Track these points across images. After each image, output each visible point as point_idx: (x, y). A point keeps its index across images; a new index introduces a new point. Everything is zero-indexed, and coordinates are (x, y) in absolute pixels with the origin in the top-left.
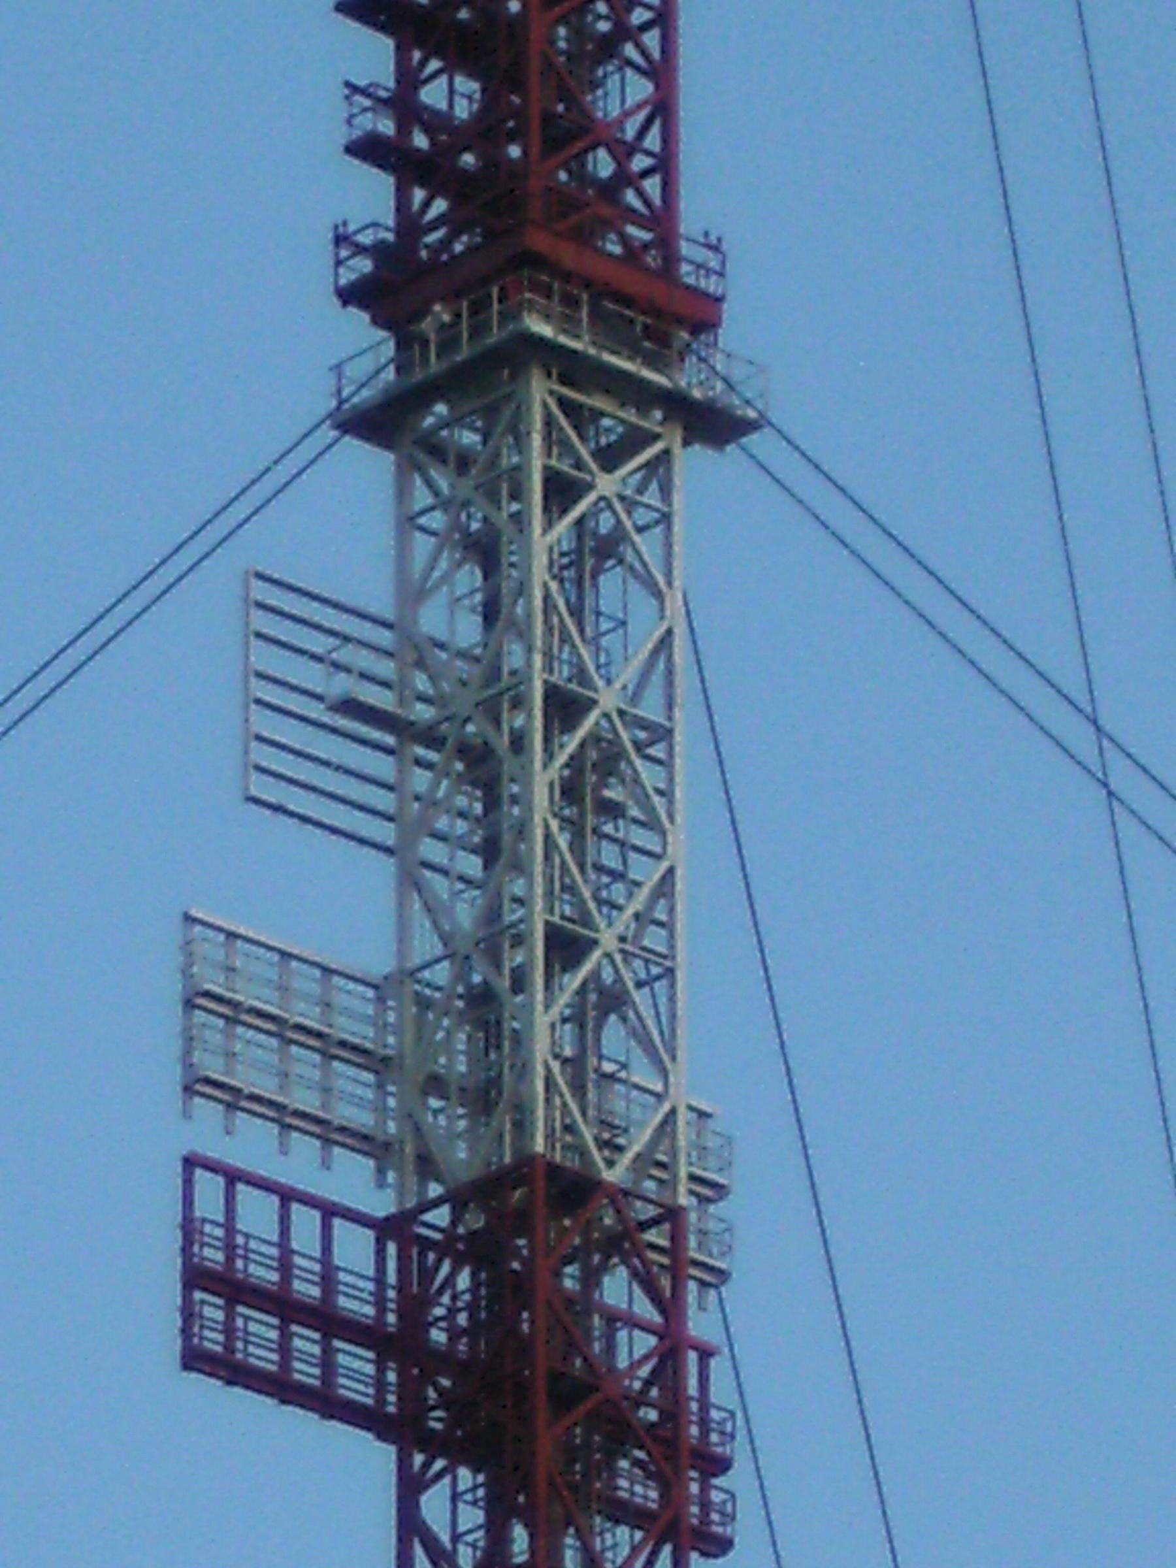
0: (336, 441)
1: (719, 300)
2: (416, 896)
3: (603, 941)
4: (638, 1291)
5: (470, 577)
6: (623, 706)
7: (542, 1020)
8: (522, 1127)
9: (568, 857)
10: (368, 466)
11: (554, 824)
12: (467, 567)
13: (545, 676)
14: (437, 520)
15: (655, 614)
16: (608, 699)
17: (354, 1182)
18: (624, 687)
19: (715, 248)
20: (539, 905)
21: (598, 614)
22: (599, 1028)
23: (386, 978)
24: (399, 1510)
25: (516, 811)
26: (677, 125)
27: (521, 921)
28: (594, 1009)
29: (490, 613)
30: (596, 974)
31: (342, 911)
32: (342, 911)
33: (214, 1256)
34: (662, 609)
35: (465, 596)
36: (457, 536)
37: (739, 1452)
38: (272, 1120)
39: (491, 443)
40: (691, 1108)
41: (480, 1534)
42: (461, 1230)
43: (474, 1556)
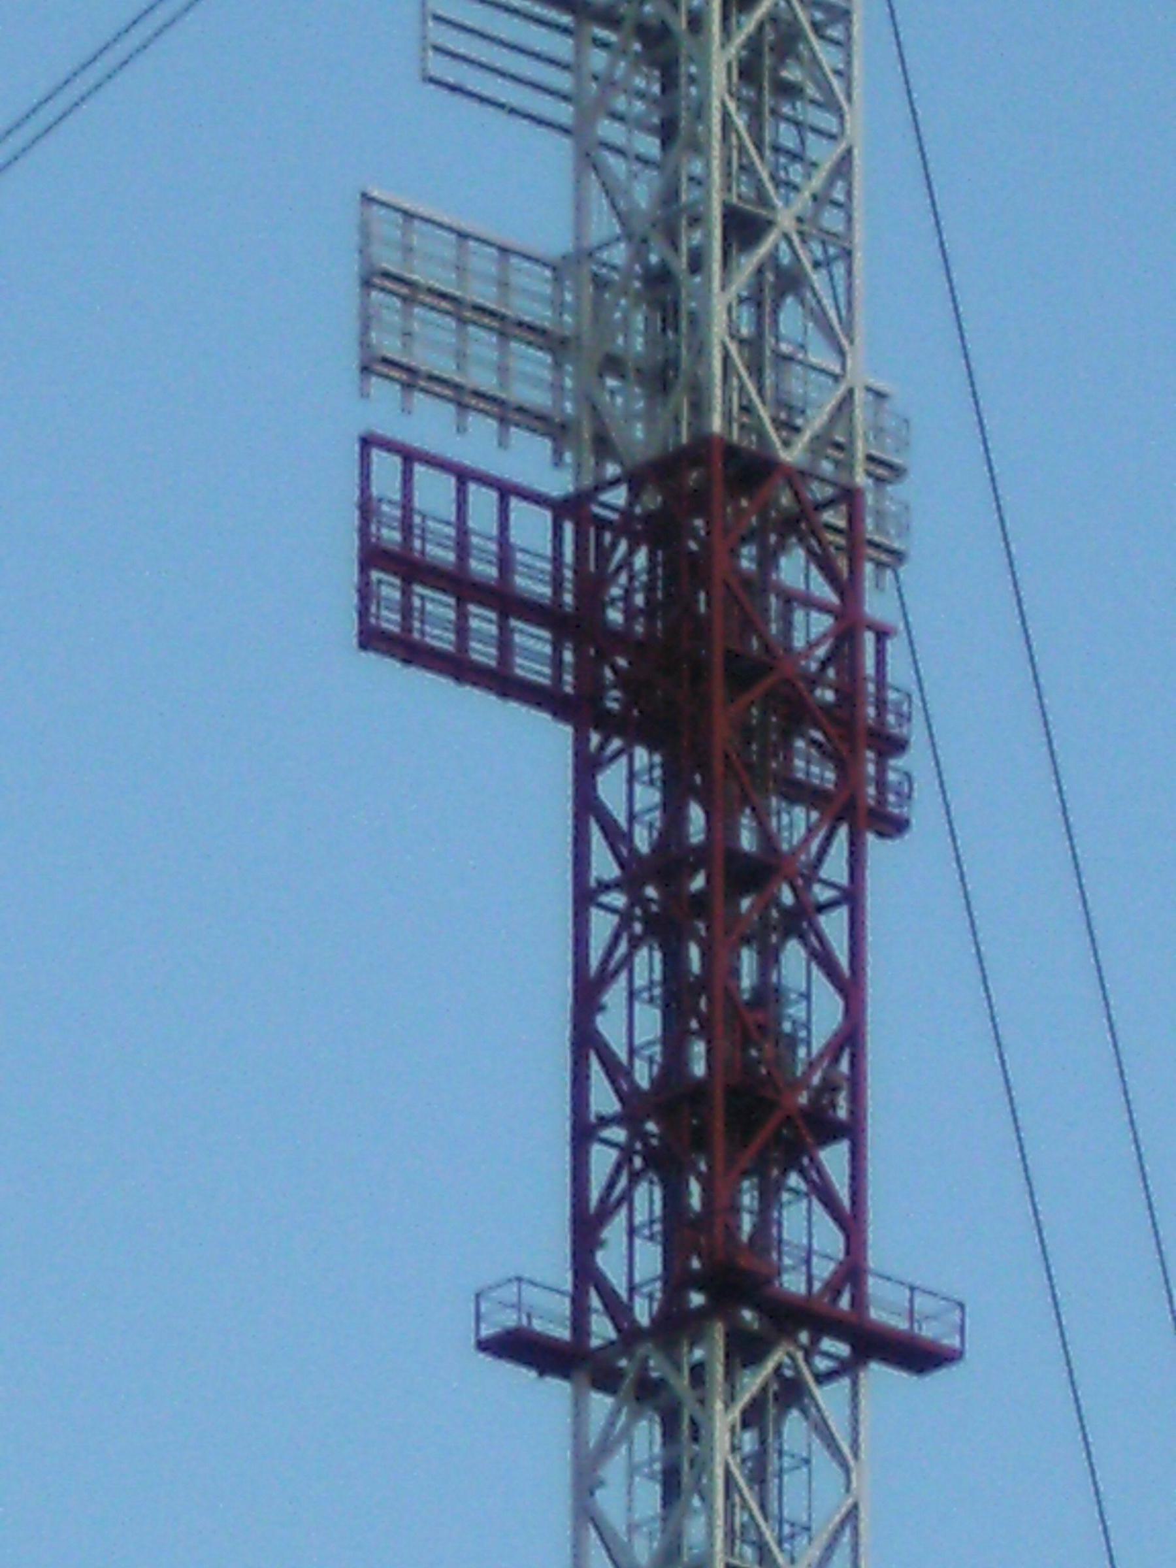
2: (593, 176)
4: (816, 972)
8: (699, 408)
11: (732, 106)
17: (531, 461)
23: (564, 257)
25: (693, 90)
31: (520, 190)
32: (520, 190)
33: (391, 536)
37: (916, 734)
38: (450, 400)
40: (869, 389)
43: (651, 1548)
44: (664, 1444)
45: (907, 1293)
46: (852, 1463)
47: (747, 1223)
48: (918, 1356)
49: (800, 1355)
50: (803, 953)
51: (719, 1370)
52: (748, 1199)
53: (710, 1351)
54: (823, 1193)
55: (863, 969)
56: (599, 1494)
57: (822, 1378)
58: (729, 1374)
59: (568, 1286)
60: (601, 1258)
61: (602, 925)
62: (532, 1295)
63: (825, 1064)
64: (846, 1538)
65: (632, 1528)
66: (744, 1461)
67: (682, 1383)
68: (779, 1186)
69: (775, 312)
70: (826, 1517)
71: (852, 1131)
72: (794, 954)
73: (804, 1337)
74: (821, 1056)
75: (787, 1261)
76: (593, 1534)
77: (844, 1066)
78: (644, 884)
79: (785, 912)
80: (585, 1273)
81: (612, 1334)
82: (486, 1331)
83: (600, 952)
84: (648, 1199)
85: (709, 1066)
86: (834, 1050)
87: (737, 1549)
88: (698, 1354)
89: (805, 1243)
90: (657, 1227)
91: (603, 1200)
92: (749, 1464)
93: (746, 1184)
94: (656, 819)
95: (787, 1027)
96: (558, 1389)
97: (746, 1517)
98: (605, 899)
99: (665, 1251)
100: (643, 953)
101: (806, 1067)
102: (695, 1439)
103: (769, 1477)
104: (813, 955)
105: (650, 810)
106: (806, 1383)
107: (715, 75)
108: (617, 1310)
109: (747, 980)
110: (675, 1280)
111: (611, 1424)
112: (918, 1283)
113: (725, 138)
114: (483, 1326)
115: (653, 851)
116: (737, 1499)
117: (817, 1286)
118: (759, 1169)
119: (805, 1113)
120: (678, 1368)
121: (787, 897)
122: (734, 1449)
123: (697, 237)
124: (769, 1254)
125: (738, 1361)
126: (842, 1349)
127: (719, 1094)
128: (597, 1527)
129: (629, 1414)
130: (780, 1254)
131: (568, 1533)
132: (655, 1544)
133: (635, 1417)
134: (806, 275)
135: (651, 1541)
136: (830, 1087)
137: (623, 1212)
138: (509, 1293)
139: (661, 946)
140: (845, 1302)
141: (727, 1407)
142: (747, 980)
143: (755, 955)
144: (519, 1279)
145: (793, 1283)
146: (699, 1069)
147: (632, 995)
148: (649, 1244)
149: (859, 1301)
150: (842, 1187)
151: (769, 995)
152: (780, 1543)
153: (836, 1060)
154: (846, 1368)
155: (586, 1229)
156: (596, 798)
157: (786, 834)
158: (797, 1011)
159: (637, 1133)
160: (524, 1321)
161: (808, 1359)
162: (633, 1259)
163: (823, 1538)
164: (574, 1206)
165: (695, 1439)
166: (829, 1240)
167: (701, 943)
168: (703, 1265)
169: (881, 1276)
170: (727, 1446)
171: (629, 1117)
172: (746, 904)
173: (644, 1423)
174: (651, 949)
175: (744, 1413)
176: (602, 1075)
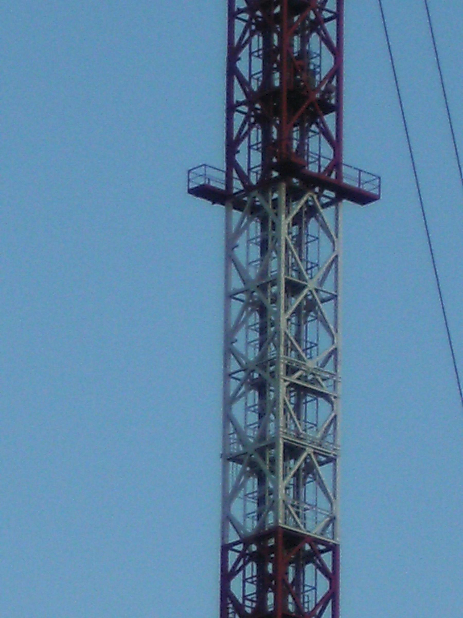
3: (309, 286)
4: (323, 45)
5: (253, 396)
6: (316, 287)
7: (282, 485)
9: (293, 413)
12: (251, 478)
13: (286, 277)
14: (241, 375)
15: (330, 343)
16: (311, 285)
18: (318, 279)
21: (308, 235)
22: (305, 478)
25: (273, 329)
26: (339, 566)
27: (275, 358)
29: (264, 247)
30: (306, 296)
34: (333, 406)
36: (249, 380)
39: (263, 349)
41: (259, 168)
42: (247, 552)
43: (258, 84)
44: (262, 231)
45: (358, 172)
46: (335, 239)
47: (295, 144)
48: (362, 198)
49: (315, 197)
50: (318, 39)
51: (283, 295)
52: (295, 135)
53: (280, 195)
54: (325, 132)
56: (237, 156)
57: (324, 206)
58: (287, 202)
59: (225, 169)
60: (239, 64)
61: (239, 26)
62: (210, 172)
63: (327, 82)
66: (293, 237)
67: (269, 207)
68: (308, 130)
69: (306, 223)
70: (325, 263)
71: (337, 108)
72: (314, 39)
73: (317, 189)
74: (325, 78)
75: (310, 160)
76: (231, 526)
77: (334, 83)
78: (257, 10)
79: (311, 21)
80: (231, 163)
81: (242, 188)
82: (192, 186)
84: (256, 135)
85: (281, 83)
86: (330, 76)
87: (290, 273)
88: (275, 196)
89: (318, 152)
91: (234, 567)
92: (295, 239)
93: (295, 129)
95: (312, 67)
96: (219, 209)
97: (293, 260)
98: (240, 108)
101: (319, 83)
102: (274, 229)
104: (318, 567)
105: (257, 167)
106: (315, 465)
108: (244, 178)
109: (296, 48)
110: (266, 166)
111: (242, 222)
112: (362, 169)
113: (286, 252)
114: (190, 184)
115: (257, 183)
116: (290, 253)
117: (322, 169)
118: (299, 123)
119: (319, 101)
120: (268, 202)
121: (312, 16)
122: (289, 233)
124: (304, 157)
125: (290, 294)
126: (332, 195)
127: (285, 94)
129: (248, 219)
130: (308, 156)
131: (222, 409)
132: (258, 271)
133: (250, 221)
134: (316, 467)
135: (254, 431)
136: (328, 91)
137: (247, 47)
138: (201, 171)
139: (262, 127)
140: (333, 176)
141: (286, 217)
142: (296, 48)
143: (299, 39)
144: (205, 165)
145: (313, 168)
146: (277, 83)
147: (250, 147)
148: (252, 585)
149: (339, 176)
150: (329, 607)
151: (305, 54)
153: (330, 82)
154: (334, 202)
155: (232, 147)
156: (230, 591)
157: (306, 605)
158: (316, 61)
159: (252, 108)
160: (207, 181)
161: (318, 198)
162: (250, 158)
163: (324, 269)
164: (227, 137)
165: (274, 229)
166: (327, 151)
167: (279, 34)
168: (277, 161)
169: (348, 166)
170: (286, 231)
171: (249, 102)
172: (296, 18)
173: (252, 391)
174: (259, 36)
175: (293, 219)
176: (239, 86)
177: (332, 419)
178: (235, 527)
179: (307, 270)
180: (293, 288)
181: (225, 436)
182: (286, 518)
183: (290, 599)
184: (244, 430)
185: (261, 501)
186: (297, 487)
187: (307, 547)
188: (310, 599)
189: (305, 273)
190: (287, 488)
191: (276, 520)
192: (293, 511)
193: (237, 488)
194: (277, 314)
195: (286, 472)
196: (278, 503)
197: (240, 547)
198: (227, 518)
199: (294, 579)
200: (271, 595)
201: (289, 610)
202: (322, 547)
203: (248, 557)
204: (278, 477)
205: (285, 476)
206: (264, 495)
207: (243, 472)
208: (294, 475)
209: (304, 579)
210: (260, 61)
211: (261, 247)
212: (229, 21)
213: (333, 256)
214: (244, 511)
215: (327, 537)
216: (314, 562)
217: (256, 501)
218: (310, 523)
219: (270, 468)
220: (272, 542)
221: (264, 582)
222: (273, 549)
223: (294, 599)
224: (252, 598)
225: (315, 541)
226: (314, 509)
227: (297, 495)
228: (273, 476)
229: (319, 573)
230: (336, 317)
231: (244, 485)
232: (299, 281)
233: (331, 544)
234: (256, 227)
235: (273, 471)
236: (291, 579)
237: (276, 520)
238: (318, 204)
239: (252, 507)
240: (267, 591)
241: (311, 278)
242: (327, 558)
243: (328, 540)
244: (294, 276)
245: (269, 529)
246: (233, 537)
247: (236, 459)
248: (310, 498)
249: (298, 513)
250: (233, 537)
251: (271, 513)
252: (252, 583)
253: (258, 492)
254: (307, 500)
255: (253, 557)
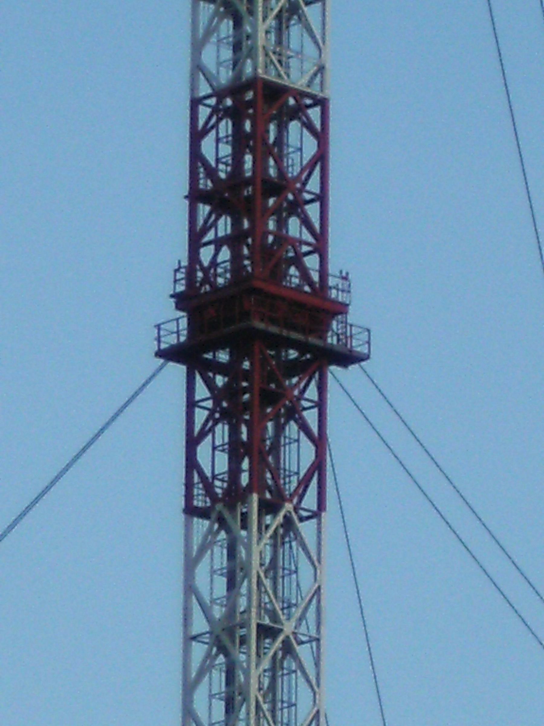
0: (161, 368)
1: (347, 305)
3: (285, 629)
4: (304, 230)
7: (262, 28)
10: (177, 371)
12: (226, 20)
16: (288, 628)
19: (345, 278)
20: (254, 614)
22: (289, 20)
24: (190, 184)
28: (287, 11)
35: (224, 38)
39: (237, 68)
41: (226, 475)
44: (234, 28)
55: (328, 182)
64: (314, 601)
65: (213, 601)
76: (202, 77)
79: (290, 203)
83: (204, 120)
90: (230, 139)
94: (228, 265)
99: (230, 459)
100: (219, 426)
103: (278, 578)
104: (304, 124)
107: (254, 558)
121: (290, 197)
123: (243, 632)
128: (204, 75)
152: (283, 609)
156: (196, 459)
157: (290, 169)
170: (258, 562)
177: (315, 592)
178: (207, 80)
179: (283, 609)
180: (266, 632)
181: (189, 486)
182: (266, 67)
183: (272, 162)
184: (209, 605)
185: (237, 47)
186: (279, 31)
187: (292, 101)
188: (295, 161)
189: (280, 612)
190: (267, 32)
191: (255, 69)
192: (274, 58)
193: (210, 31)
194: (254, 26)
195: (267, 13)
196: (257, 49)
197: (212, 101)
198: (198, 68)
199: (276, 138)
200: (249, 158)
201: (270, 176)
202: (308, 102)
203: (222, 113)
204: (256, 20)
205: (265, 18)
206: (235, 571)
207: (216, 13)
208: (271, 537)
209: (289, 42)
210: (226, 456)
211: (226, 703)
212: (187, 472)
213: (314, 711)
214: (217, 59)
215: (315, 90)
216: (299, 119)
217: (231, 48)
218: (294, 73)
219: (248, 9)
220: (249, 95)
221: (240, 143)
222: (251, 104)
223: (276, 161)
224: (223, 478)
225: (299, 95)
226: (300, 56)
227: (279, 42)
228: (251, 18)
229: (305, 131)
230: (319, 544)
231: (216, 29)
232: (271, 625)
233: (319, 98)
234: (222, 553)
235: (251, 12)
236: (272, 139)
237: (255, 69)
238: (295, 517)
239: (227, 54)
240: (243, 154)
241: (288, 619)
242: (314, 114)
243: (317, 93)
244: (267, 621)
245: (247, 81)
246: (204, 89)
247: (203, 513)
248: (294, 44)
249: (280, 62)
250: (204, 89)
251: (249, 61)
252: (223, 451)
253: (234, 37)
254: (291, 46)
255: (228, 113)
